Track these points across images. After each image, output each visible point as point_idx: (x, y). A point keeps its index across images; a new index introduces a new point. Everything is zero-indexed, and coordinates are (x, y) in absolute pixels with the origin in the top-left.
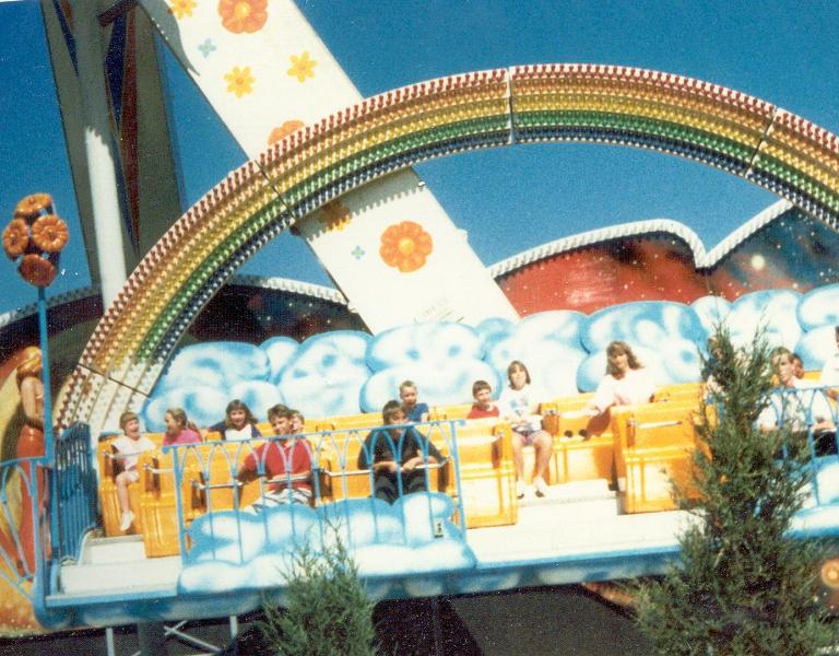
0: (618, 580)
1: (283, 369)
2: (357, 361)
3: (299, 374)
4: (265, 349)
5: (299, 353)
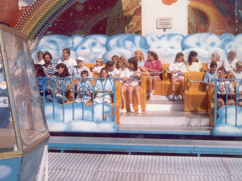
0: (47, 124)
1: (78, 46)
2: (103, 45)
3: (83, 48)
4: (73, 38)
5: (84, 41)
